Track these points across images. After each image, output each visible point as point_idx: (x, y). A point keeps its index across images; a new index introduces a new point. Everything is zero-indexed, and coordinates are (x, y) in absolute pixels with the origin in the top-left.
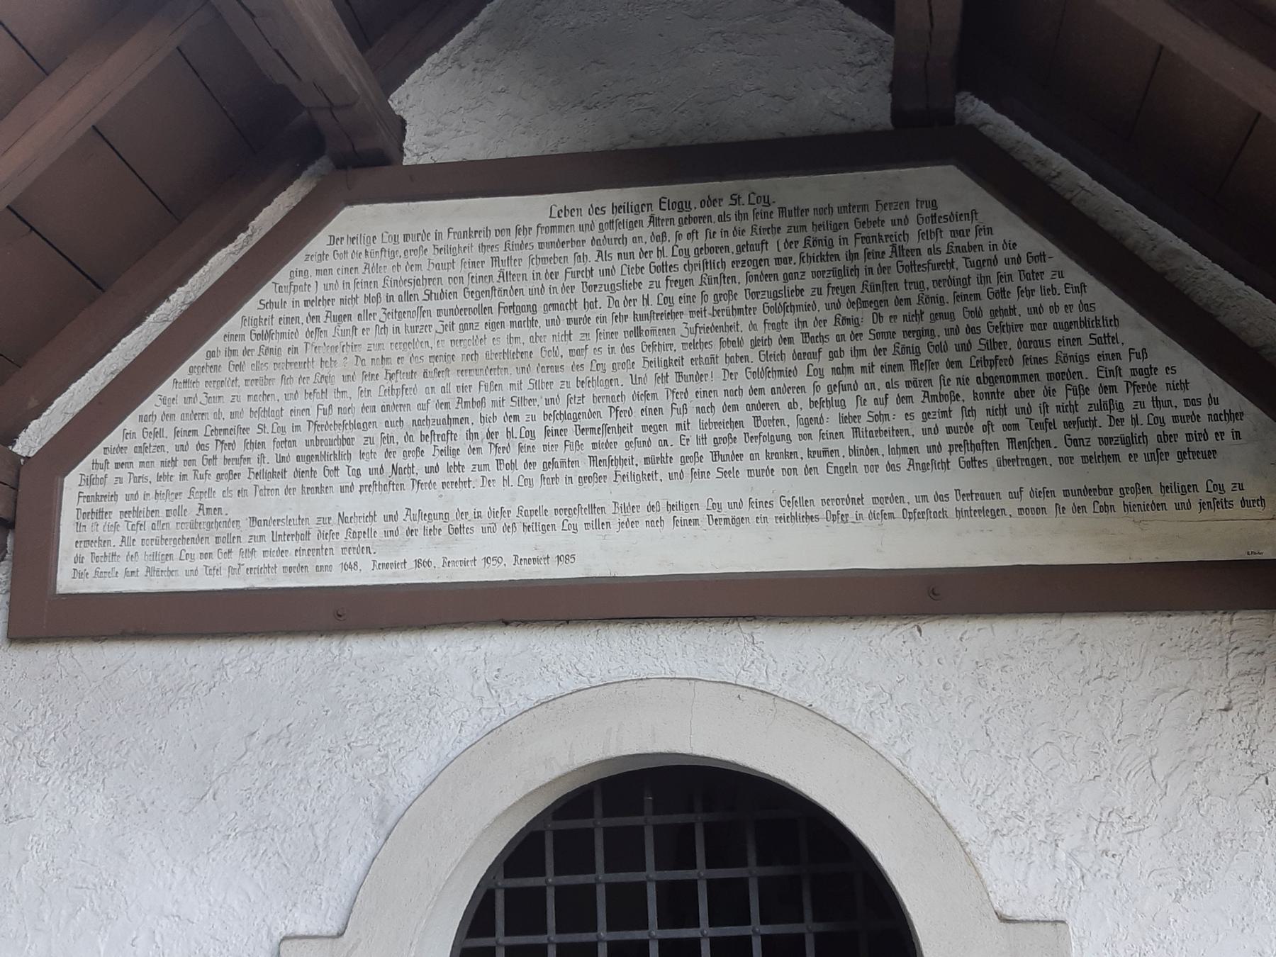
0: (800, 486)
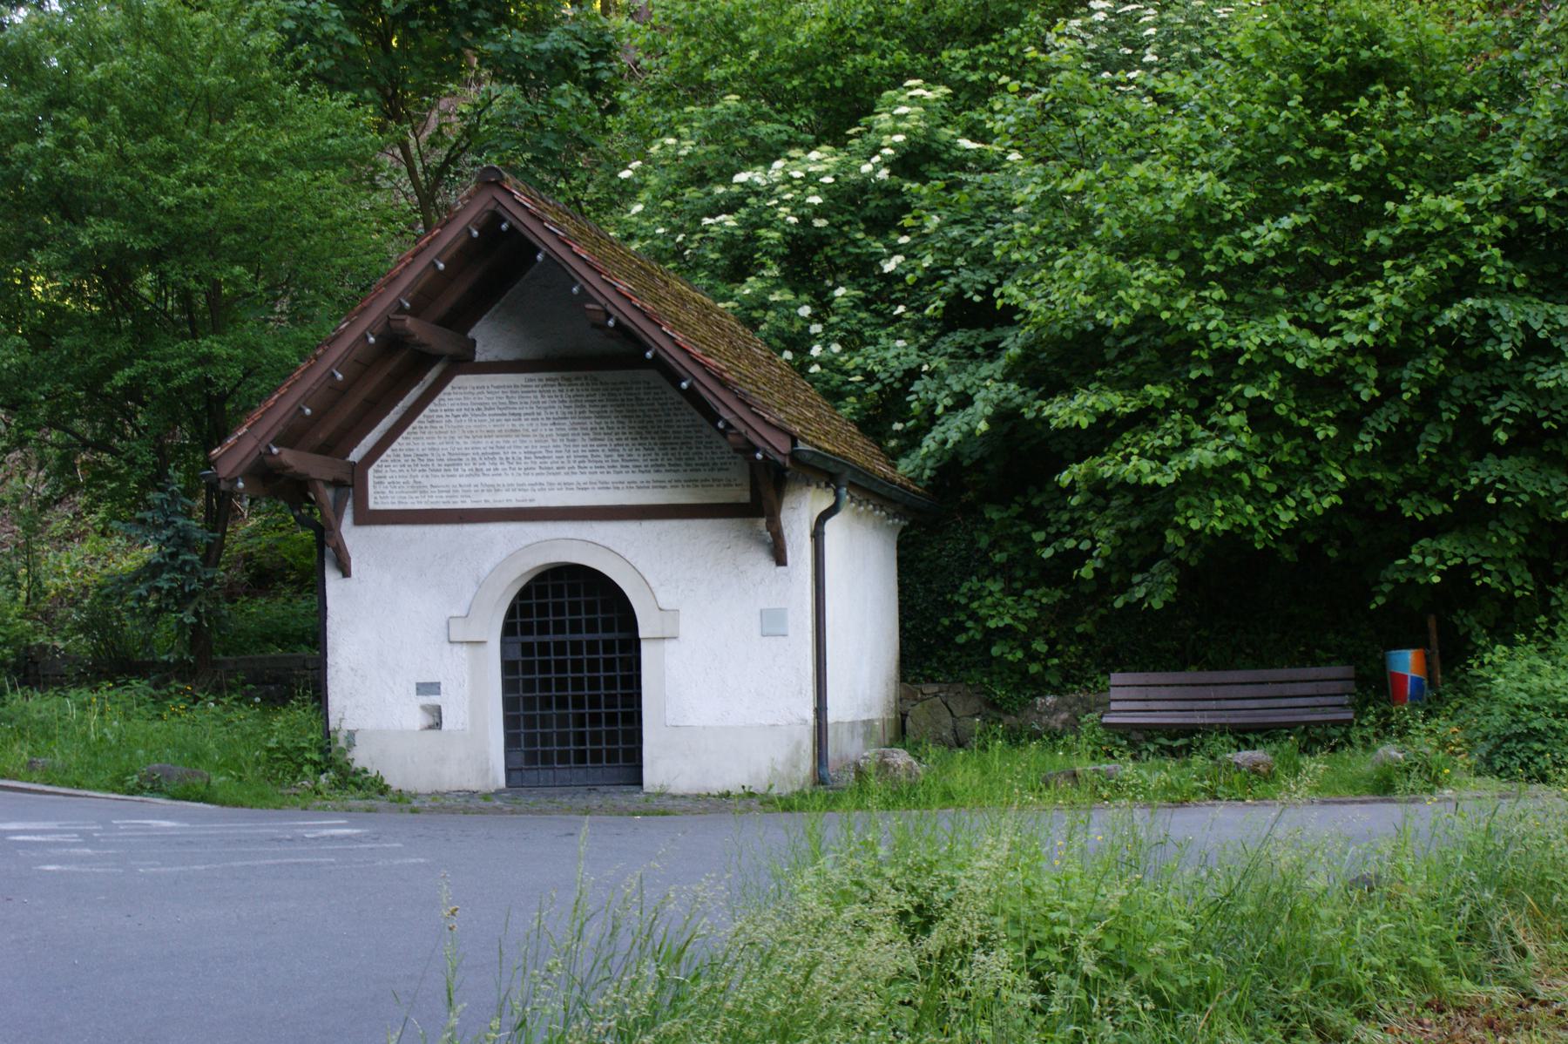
0: (605, 478)
